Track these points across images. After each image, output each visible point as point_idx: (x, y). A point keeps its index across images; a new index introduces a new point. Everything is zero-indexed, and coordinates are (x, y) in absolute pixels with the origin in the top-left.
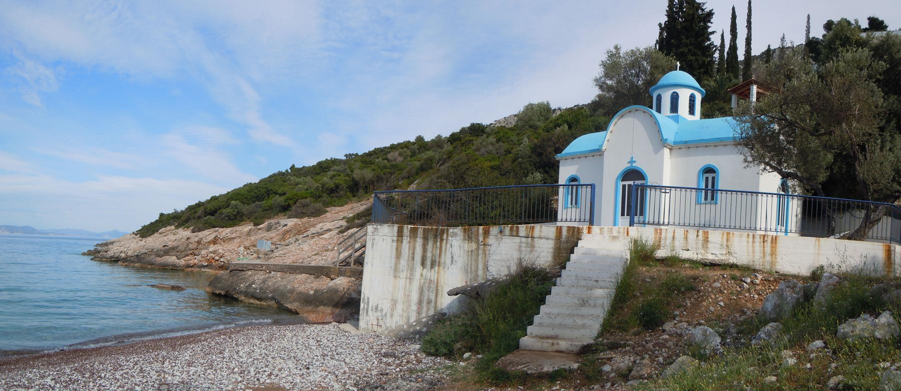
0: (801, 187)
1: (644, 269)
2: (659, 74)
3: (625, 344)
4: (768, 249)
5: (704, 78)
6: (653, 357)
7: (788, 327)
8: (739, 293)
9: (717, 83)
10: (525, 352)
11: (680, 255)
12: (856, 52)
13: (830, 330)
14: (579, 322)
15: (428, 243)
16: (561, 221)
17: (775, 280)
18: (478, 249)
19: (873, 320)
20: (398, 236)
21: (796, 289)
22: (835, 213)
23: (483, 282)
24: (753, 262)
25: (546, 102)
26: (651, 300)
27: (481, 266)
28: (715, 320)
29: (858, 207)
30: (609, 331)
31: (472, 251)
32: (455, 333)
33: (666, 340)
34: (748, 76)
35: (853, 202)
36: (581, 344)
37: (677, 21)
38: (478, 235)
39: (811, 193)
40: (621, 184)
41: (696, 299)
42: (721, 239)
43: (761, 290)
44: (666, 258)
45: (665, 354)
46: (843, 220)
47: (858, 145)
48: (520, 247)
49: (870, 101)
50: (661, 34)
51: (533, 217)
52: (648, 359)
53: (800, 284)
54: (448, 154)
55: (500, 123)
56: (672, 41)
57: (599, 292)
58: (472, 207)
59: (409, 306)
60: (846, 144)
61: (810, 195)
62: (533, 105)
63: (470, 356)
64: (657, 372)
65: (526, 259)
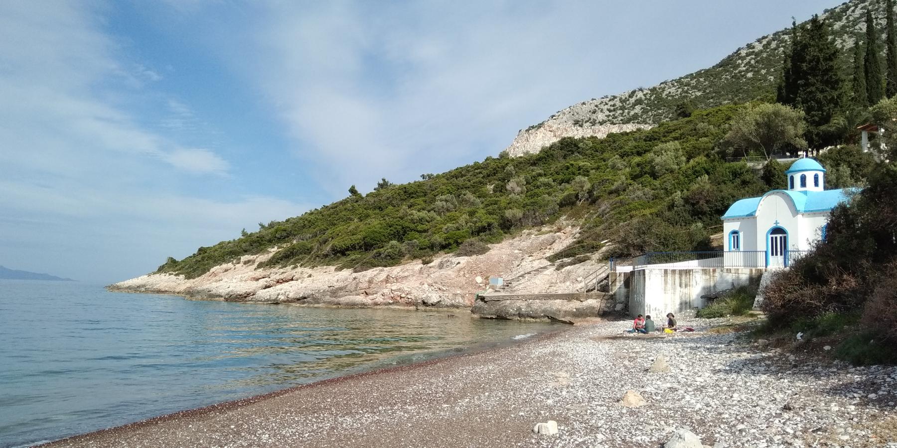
18: (710, 278)
20: (665, 274)
31: (707, 279)
40: (770, 236)
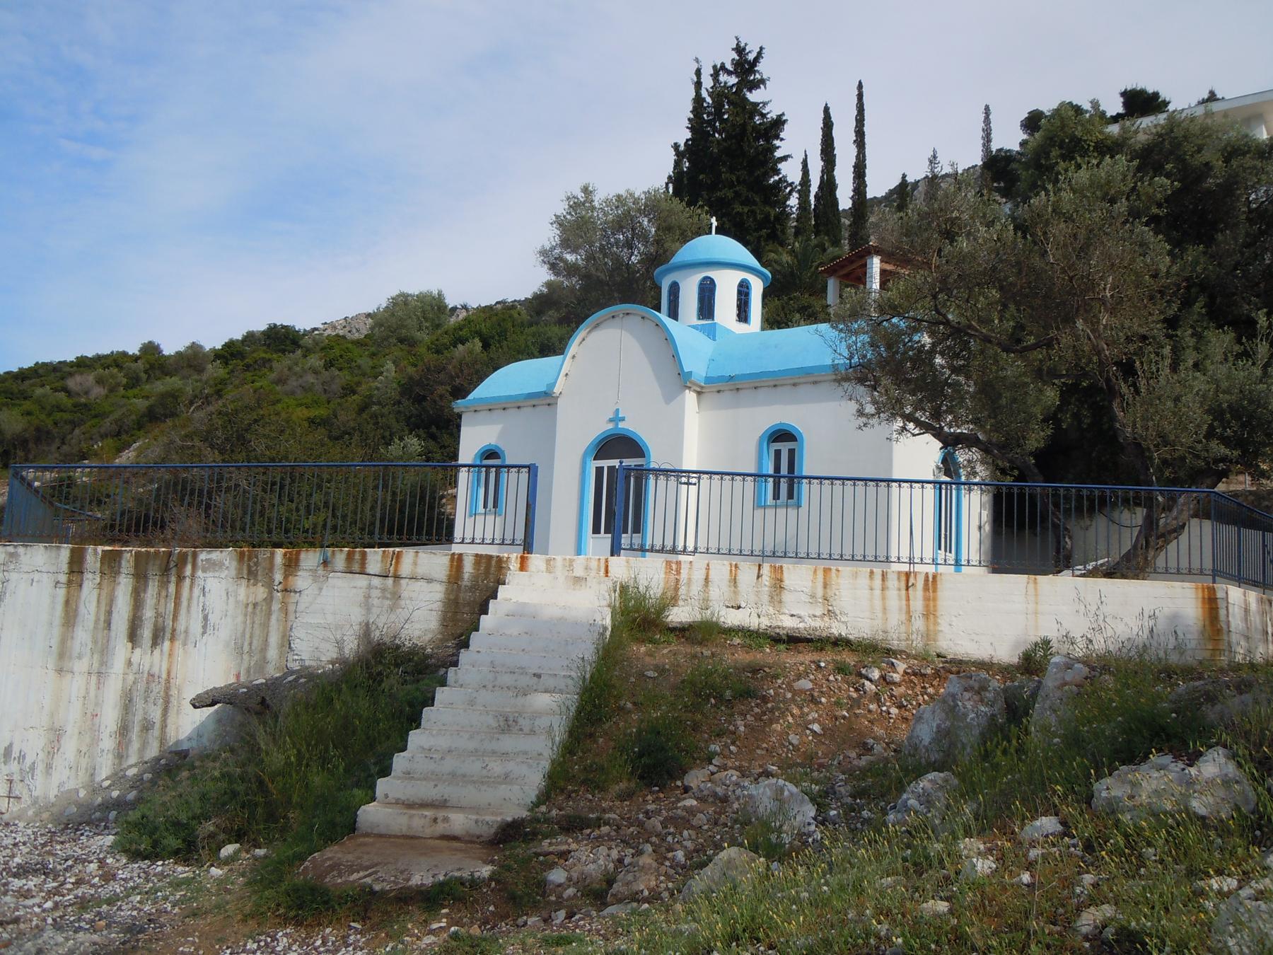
0: (987, 463)
1: (643, 649)
2: (673, 241)
3: (599, 819)
4: (918, 604)
5: (768, 248)
6: (663, 849)
7: (972, 783)
8: (855, 703)
9: (796, 257)
10: (371, 840)
11: (722, 619)
12: (1098, 166)
13: (1075, 793)
14: (497, 767)
15: (146, 586)
16: (462, 542)
17: (937, 674)
18: (269, 600)
19: (1183, 769)
20: (71, 572)
21: (988, 695)
22: (1070, 515)
23: (278, 675)
24: (885, 632)
25: (435, 293)
26: (657, 718)
27: (274, 639)
28: (802, 765)
29: (1126, 502)
30: (562, 790)
31: (255, 605)
32: (203, 797)
33: (691, 811)
34: (862, 239)
35: (1113, 491)
36: (499, 819)
37: (711, 138)
38: (271, 568)
39: (1011, 476)
40: (593, 465)
41: (758, 718)
42: (810, 583)
43: (905, 696)
44: (690, 625)
45: (689, 844)
46: (1091, 533)
47: (1116, 364)
48: (368, 597)
49: (1139, 264)
50: (677, 164)
51: (400, 532)
52: (650, 855)
53: (996, 683)
54: (216, 385)
55: (334, 328)
56: (701, 177)
57: (543, 701)
58: (263, 506)
59: (95, 740)
60: (1087, 365)
61: (1008, 481)
62: (409, 295)
63: (236, 852)
64: (670, 885)
65: (381, 625)
